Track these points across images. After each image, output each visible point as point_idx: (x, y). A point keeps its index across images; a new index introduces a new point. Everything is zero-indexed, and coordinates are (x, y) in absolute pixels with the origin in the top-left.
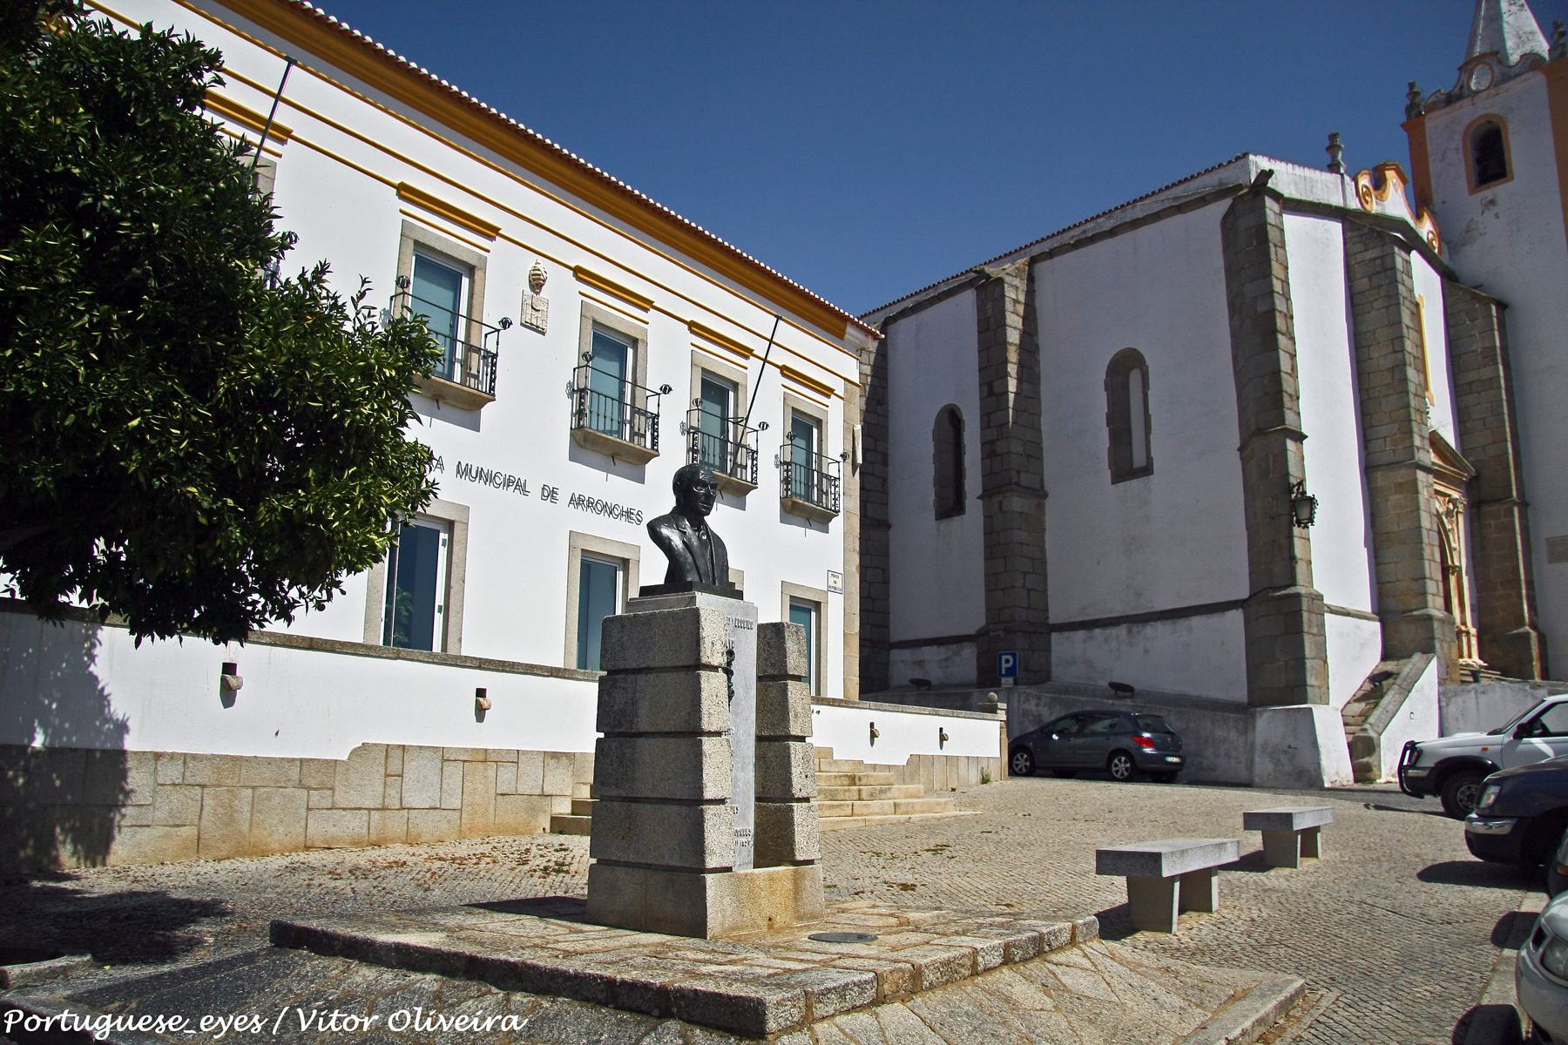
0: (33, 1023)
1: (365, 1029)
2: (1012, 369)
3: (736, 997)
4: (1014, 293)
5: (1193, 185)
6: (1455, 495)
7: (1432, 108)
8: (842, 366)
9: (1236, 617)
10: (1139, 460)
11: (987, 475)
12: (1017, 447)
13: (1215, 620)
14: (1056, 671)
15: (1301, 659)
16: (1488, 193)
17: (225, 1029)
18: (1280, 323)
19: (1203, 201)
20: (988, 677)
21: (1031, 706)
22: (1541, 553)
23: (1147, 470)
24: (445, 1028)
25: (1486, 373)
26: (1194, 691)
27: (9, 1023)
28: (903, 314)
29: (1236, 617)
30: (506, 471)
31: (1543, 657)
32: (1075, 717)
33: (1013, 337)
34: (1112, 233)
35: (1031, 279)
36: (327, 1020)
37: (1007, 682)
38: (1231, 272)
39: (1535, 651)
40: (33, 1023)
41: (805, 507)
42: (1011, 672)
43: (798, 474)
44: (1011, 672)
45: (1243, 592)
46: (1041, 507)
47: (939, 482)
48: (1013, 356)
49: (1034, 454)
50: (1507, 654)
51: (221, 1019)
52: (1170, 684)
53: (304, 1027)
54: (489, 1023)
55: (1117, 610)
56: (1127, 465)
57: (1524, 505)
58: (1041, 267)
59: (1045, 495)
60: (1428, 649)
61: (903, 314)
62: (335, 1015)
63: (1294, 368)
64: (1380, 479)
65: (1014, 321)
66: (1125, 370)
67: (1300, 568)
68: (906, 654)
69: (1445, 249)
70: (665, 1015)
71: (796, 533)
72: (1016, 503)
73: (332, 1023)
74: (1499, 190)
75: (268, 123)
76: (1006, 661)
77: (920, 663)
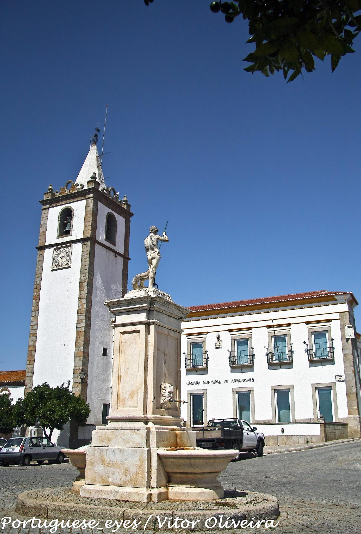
0: (16, 524)
1: (24, 527)
17: (118, 527)
27: (4, 524)
30: (214, 380)
36: (172, 522)
40: (16, 524)
51: (116, 522)
73: (175, 524)
75: (274, 328)
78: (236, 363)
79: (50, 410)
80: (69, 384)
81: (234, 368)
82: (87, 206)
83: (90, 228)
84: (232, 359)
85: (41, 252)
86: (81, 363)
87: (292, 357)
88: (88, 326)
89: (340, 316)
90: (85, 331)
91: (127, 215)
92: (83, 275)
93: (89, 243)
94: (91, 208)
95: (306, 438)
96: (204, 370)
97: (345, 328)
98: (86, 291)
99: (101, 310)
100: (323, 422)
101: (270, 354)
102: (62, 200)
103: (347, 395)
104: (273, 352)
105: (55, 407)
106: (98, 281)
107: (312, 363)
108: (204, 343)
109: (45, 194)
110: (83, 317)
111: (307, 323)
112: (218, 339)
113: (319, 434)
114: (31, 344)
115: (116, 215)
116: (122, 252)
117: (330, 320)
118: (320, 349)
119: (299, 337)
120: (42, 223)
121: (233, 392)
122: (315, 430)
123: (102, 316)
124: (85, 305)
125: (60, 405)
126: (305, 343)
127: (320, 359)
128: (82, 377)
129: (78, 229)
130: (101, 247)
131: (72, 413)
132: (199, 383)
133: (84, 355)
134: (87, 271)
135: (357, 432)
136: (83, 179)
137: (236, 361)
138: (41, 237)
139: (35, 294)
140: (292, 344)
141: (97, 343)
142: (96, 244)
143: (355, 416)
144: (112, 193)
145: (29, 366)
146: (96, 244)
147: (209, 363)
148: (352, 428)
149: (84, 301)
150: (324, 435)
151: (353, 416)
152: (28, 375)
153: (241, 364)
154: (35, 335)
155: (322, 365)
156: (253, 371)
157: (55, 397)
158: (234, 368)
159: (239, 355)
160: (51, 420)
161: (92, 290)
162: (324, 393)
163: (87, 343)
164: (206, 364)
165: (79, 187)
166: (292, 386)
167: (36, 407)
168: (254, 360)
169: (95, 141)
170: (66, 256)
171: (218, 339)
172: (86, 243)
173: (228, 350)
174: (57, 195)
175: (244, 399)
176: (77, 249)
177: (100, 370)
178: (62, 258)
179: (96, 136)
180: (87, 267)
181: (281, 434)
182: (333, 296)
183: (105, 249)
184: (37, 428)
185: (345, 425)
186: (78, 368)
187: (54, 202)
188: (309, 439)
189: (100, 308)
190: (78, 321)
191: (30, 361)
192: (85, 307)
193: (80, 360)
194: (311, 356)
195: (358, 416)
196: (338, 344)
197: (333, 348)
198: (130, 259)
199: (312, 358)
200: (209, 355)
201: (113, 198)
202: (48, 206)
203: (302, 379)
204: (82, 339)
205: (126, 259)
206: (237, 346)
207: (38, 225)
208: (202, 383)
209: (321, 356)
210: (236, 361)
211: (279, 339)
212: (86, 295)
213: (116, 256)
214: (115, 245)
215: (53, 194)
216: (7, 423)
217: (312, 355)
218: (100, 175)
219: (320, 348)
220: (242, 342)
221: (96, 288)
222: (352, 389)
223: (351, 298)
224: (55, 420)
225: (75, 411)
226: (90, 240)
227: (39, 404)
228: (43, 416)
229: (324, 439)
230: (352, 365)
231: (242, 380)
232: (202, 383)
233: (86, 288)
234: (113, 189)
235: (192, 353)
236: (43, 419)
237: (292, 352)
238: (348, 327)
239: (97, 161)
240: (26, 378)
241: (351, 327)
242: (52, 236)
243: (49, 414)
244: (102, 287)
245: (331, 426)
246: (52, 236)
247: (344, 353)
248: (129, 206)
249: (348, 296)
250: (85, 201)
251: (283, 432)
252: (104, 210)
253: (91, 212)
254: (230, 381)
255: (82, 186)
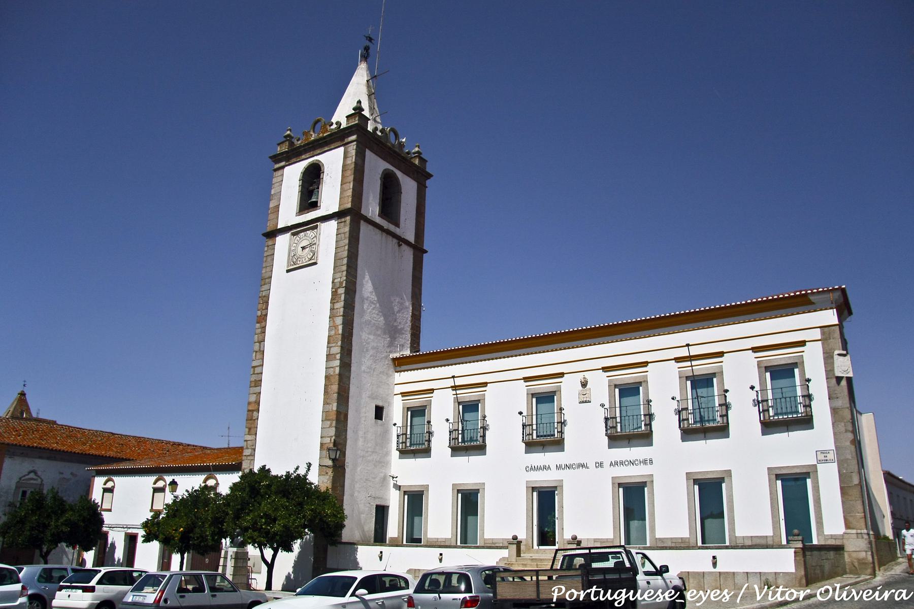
3: (355, 174)
17: (704, 599)
24: (856, 599)
51: (701, 592)
53: (759, 598)
54: (886, 595)
62: (781, 589)
70: (386, 317)
73: (778, 595)
75: (691, 361)
78: (619, 430)
79: (266, 516)
80: (309, 469)
81: (615, 439)
82: (345, 157)
83: (350, 193)
84: (610, 423)
85: (270, 242)
86: (332, 432)
87: (727, 415)
88: (346, 365)
89: (823, 333)
90: (340, 375)
91: (421, 175)
92: (338, 275)
93: (348, 218)
94: (352, 160)
95: (763, 578)
96: (558, 444)
97: (832, 357)
98: (342, 304)
99: (372, 337)
100: (800, 545)
101: (684, 412)
102: (306, 152)
103: (842, 488)
104: (690, 407)
105: (276, 510)
106: (367, 287)
107: (768, 427)
108: (557, 393)
109: (279, 144)
110: (336, 350)
111: (755, 349)
112: (584, 384)
113: (793, 570)
114: (253, 398)
115: (399, 174)
116: (411, 238)
117: (802, 343)
118: (783, 400)
119: (741, 379)
120: (273, 192)
121: (613, 484)
122: (784, 561)
123: (373, 348)
124: (340, 327)
125: (287, 507)
126: (752, 388)
127: (784, 418)
128: (333, 457)
129: (331, 197)
130: (371, 227)
131: (310, 521)
132: (549, 468)
133: (339, 417)
134: (344, 268)
135: (865, 564)
136: (341, 115)
137: (619, 425)
138: (271, 216)
139: (259, 313)
140: (727, 391)
141: (364, 396)
142: (362, 222)
143: (859, 531)
144: (392, 137)
145: (248, 437)
146: (362, 222)
147: (566, 430)
148: (854, 555)
149: (339, 321)
150: (803, 573)
151: (854, 531)
152: (247, 452)
153: (628, 431)
154: (258, 383)
155: (788, 431)
156: (650, 444)
157: (276, 493)
158: (615, 439)
159: (624, 414)
160: (267, 533)
161: (353, 302)
162: (794, 486)
163: (343, 396)
164: (561, 432)
165: (334, 126)
166: (729, 473)
167: (242, 509)
168: (653, 423)
169: (365, 58)
170: (311, 245)
171: (584, 384)
172: (343, 220)
173: (603, 405)
174: (298, 143)
175: (634, 499)
176: (329, 229)
177: (370, 445)
178: (303, 248)
179: (367, 49)
180: (345, 261)
181: (710, 569)
182: (806, 294)
183: (378, 231)
184: (235, 549)
185: (839, 549)
186: (327, 440)
187: (292, 156)
188: (771, 579)
189: (369, 334)
190: (329, 357)
191: (250, 429)
192: (340, 332)
193: (331, 426)
194: (766, 413)
195: (865, 531)
196: (820, 389)
197: (809, 397)
198: (426, 252)
199: (767, 417)
200: (567, 416)
201: (393, 145)
202: (283, 164)
203: (749, 458)
204: (335, 387)
205: (418, 250)
206: (620, 397)
207: (268, 197)
208: (553, 467)
209: (786, 414)
210: (619, 425)
211: (701, 382)
212: (342, 309)
213: (400, 245)
214: (397, 225)
215: (292, 144)
216: (202, 537)
217: (768, 410)
218: (371, 109)
219: (785, 398)
220: (629, 391)
221: (363, 300)
222: (851, 477)
223: (842, 300)
224: (275, 534)
225: (315, 517)
226: (352, 215)
227: (248, 504)
228: (254, 527)
229: (804, 581)
230: (850, 429)
231: (631, 462)
232: (553, 467)
233: (343, 297)
234: (392, 130)
235: (534, 413)
236: (254, 531)
237: (726, 406)
238: (839, 355)
239: (368, 86)
240: (244, 458)
241: (844, 355)
242: (288, 211)
243: (265, 524)
244: (374, 297)
245: (815, 553)
246: (288, 211)
247: (834, 405)
248: (423, 161)
249: (838, 294)
250: (342, 149)
251: (715, 565)
252: (376, 166)
253: (353, 166)
254: (606, 464)
255: (339, 124)
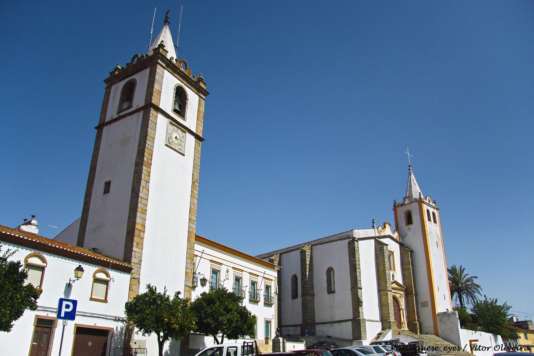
2: (307, 270)
4: (308, 253)
5: (343, 234)
6: (401, 293)
7: (398, 206)
8: (273, 274)
9: (350, 322)
10: (333, 290)
11: (303, 292)
12: (308, 286)
13: (347, 323)
14: (316, 333)
15: (361, 331)
16: (409, 227)
18: (357, 266)
19: (344, 239)
20: (303, 334)
21: (311, 340)
22: (420, 305)
23: (334, 292)
25: (408, 267)
26: (343, 337)
28: (284, 253)
29: (350, 322)
31: (420, 328)
32: (319, 343)
33: (308, 263)
34: (328, 242)
35: (312, 250)
37: (307, 335)
38: (350, 255)
39: (418, 327)
41: (268, 304)
42: (307, 333)
43: (267, 297)
44: (307, 333)
45: (352, 318)
46: (313, 298)
47: (293, 291)
48: (308, 267)
49: (312, 287)
50: (412, 328)
52: (339, 336)
55: (328, 320)
56: (331, 291)
57: (416, 295)
58: (314, 247)
59: (314, 296)
60: (390, 328)
61: (284, 253)
63: (360, 275)
64: (382, 293)
65: (308, 259)
66: (330, 271)
67: (361, 314)
68: (285, 328)
69: (401, 238)
71: (267, 308)
72: (308, 298)
74: (411, 226)
76: (306, 331)
77: (289, 330)
